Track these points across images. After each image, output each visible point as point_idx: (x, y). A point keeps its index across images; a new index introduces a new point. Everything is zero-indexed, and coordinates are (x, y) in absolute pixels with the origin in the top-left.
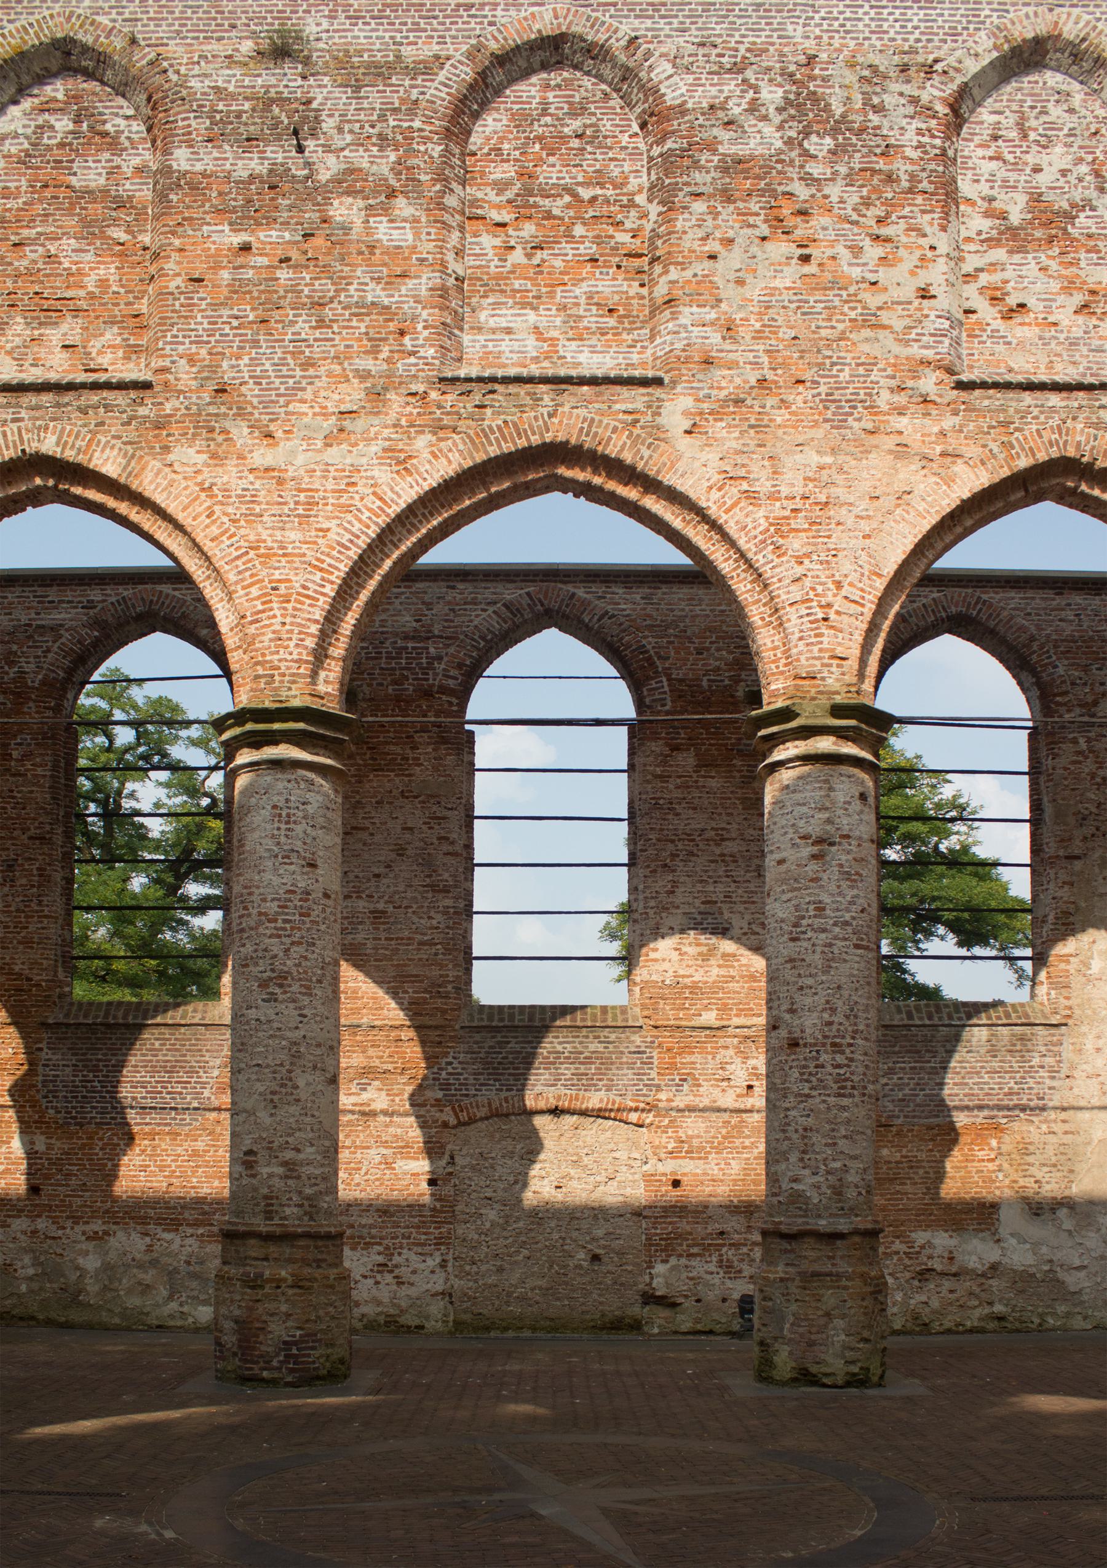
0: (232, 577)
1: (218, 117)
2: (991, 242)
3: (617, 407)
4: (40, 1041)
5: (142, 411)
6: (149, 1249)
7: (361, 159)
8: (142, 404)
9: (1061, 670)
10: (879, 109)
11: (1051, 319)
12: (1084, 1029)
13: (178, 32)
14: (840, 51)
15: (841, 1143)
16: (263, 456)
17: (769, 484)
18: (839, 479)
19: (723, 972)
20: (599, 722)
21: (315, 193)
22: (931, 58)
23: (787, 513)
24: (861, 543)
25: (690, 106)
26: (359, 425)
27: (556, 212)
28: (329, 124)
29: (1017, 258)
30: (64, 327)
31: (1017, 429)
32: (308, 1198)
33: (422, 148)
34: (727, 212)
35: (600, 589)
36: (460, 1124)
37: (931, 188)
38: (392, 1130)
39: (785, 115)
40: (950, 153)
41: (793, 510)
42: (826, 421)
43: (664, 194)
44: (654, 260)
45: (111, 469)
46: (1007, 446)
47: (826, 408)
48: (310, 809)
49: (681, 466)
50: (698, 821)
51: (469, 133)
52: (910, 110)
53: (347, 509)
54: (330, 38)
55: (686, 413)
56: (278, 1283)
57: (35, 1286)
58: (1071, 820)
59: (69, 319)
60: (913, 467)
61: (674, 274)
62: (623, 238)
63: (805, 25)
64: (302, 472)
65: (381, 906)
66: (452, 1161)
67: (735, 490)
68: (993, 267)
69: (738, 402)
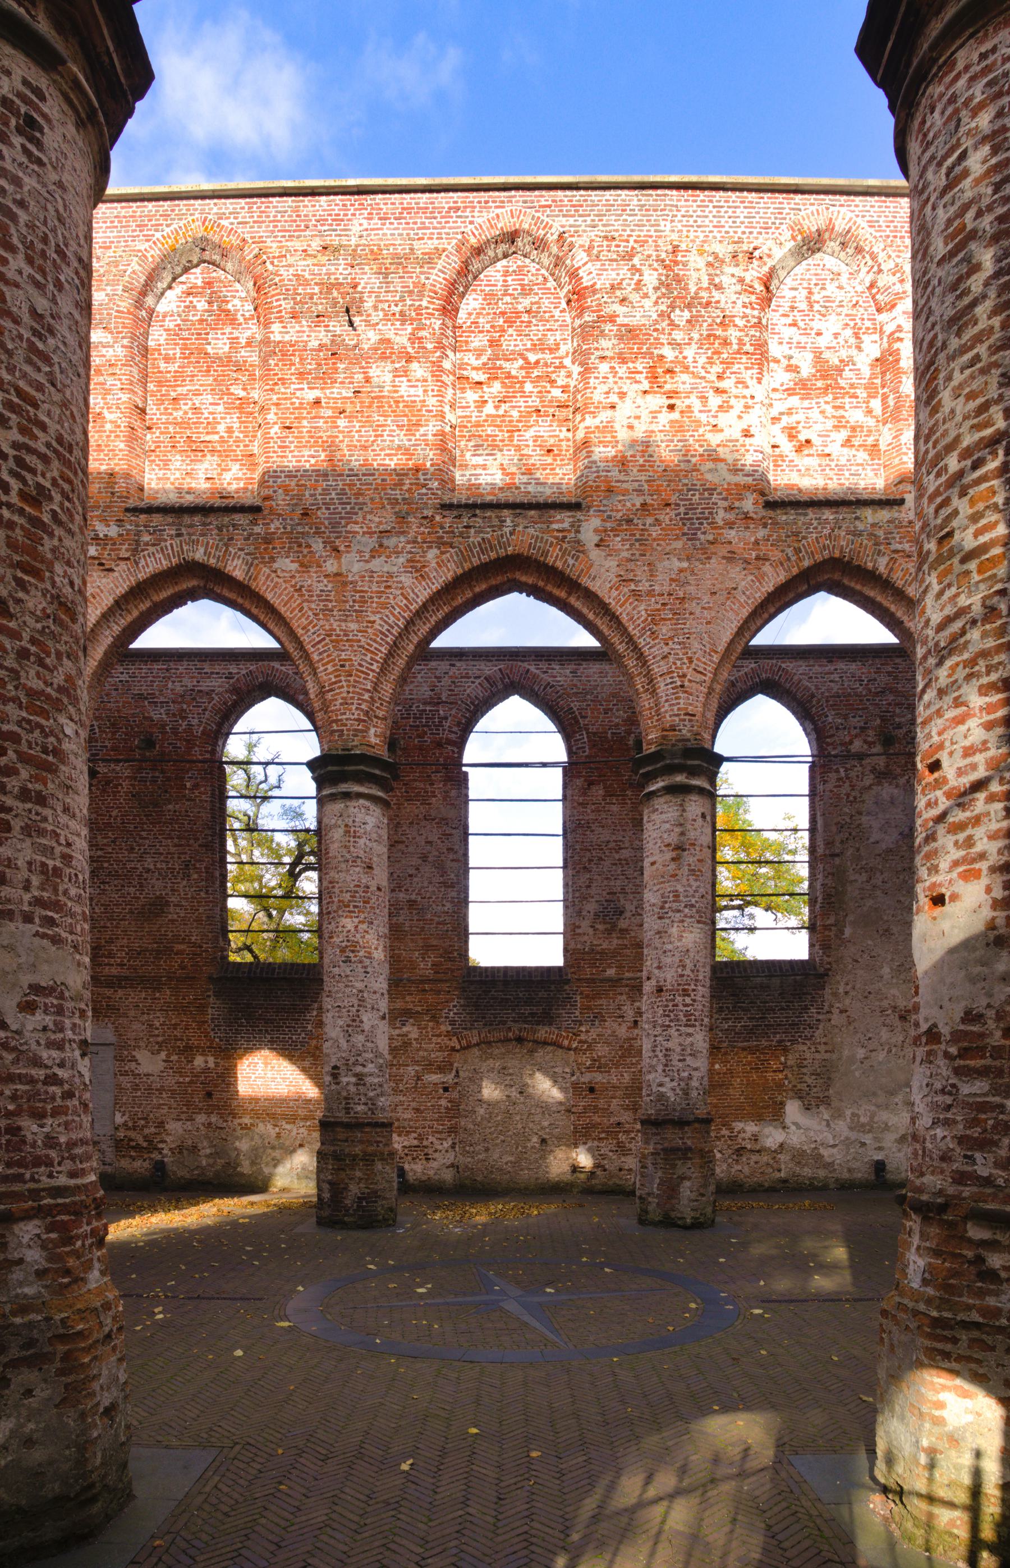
0: (315, 657)
1: (299, 298)
2: (790, 392)
3: (555, 526)
4: (209, 990)
5: (257, 529)
6: (278, 1136)
7: (389, 331)
8: (256, 524)
9: (830, 719)
10: (719, 287)
11: (827, 451)
12: (838, 978)
13: (273, 232)
14: (693, 241)
15: (688, 1058)
16: (331, 566)
17: (647, 584)
18: (691, 579)
19: (620, 942)
20: (544, 765)
21: (359, 358)
22: (752, 246)
23: (659, 606)
24: (703, 628)
25: (598, 287)
26: (391, 542)
27: (514, 373)
28: (368, 305)
29: (806, 403)
30: (206, 465)
31: (804, 538)
32: (371, 1099)
33: (428, 322)
34: (622, 370)
35: (544, 666)
36: (463, 1048)
37: (751, 349)
38: (421, 1053)
39: (659, 293)
40: (764, 322)
41: (663, 604)
42: (684, 534)
43: (581, 356)
44: (576, 410)
45: (238, 574)
46: (798, 551)
47: (684, 524)
48: (368, 828)
49: (593, 572)
50: (605, 835)
51: (457, 310)
52: (738, 287)
53: (384, 606)
54: (369, 235)
55: (596, 531)
56: (354, 1157)
57: (211, 1161)
58: (834, 829)
59: (209, 457)
60: (738, 569)
61: (589, 421)
62: (556, 393)
63: (672, 221)
64: (357, 578)
65: (413, 897)
66: (457, 1075)
67: (626, 590)
68: (789, 412)
69: (629, 521)
